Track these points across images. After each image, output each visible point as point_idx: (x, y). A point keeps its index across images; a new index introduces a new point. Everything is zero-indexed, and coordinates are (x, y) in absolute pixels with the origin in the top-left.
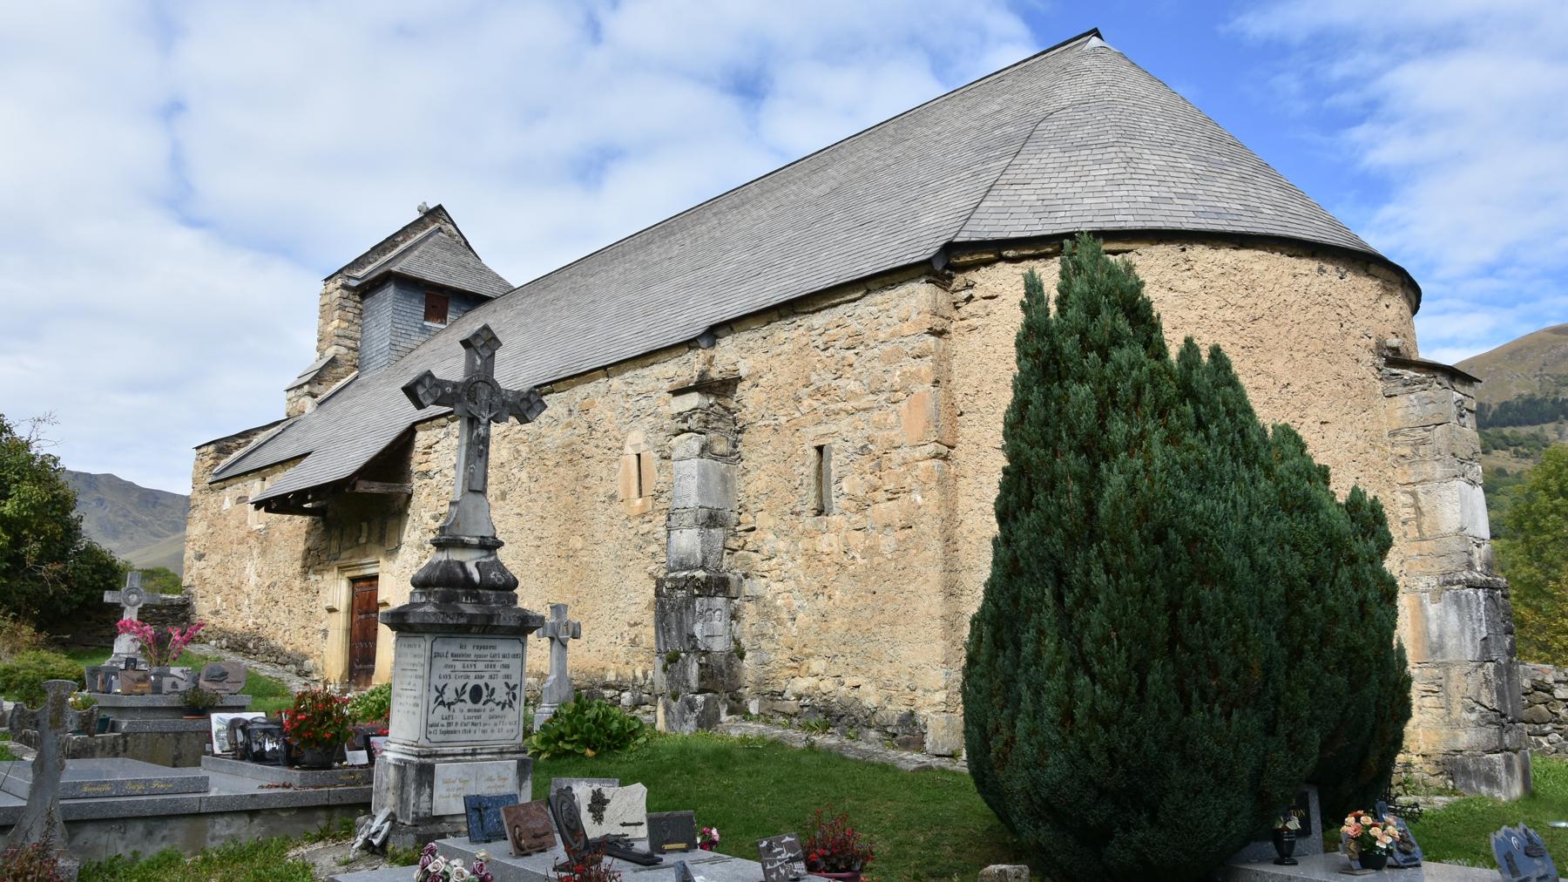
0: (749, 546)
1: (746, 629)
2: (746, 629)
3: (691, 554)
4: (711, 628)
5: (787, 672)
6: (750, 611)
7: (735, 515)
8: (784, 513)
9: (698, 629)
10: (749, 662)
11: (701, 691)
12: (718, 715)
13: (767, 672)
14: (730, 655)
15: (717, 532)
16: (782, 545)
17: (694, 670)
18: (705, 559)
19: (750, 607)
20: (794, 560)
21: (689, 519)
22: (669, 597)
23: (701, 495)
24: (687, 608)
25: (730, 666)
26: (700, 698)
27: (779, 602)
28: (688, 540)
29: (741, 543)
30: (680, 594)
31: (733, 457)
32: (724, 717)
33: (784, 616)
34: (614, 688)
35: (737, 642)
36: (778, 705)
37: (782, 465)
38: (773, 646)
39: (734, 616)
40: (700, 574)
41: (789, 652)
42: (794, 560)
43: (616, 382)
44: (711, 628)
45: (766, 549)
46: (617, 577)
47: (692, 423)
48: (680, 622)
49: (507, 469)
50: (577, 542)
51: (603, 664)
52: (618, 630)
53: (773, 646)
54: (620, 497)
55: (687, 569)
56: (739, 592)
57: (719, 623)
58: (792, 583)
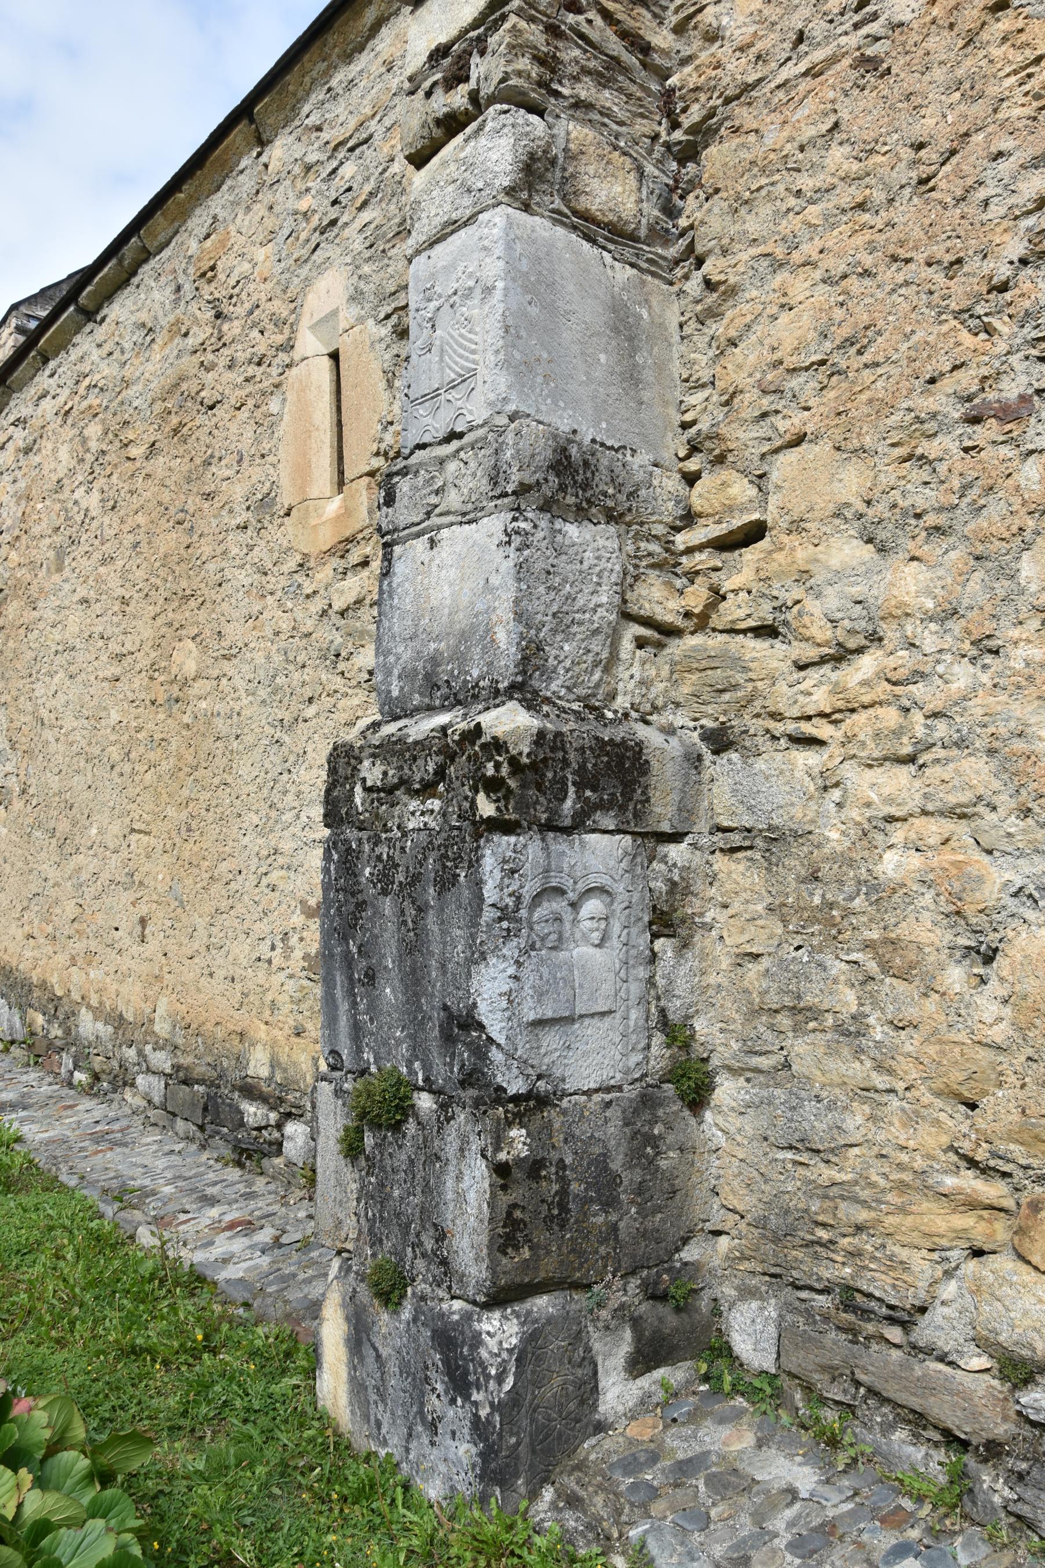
0: (733, 610)
1: (716, 983)
2: (716, 983)
3: (476, 633)
4: (562, 984)
5: (944, 1222)
6: (735, 897)
7: (673, 483)
8: (926, 425)
9: (490, 989)
10: (730, 1121)
11: (500, 1297)
12: (589, 1390)
13: (826, 1191)
14: (647, 1101)
15: (592, 542)
16: (910, 583)
17: (468, 1192)
18: (532, 655)
19: (737, 874)
20: (987, 648)
21: (465, 478)
22: (375, 827)
23: (521, 369)
24: (446, 882)
25: (644, 1145)
26: (499, 1332)
27: (893, 864)
28: (463, 576)
29: (696, 597)
30: (419, 815)
31: (657, 244)
32: (617, 1392)
33: (924, 929)
34: (262, 1098)
35: (675, 1032)
36: (883, 1362)
37: (908, 213)
38: (859, 1070)
39: (666, 921)
40: (509, 721)
41: (955, 1121)
42: (987, 648)
43: (281, 151)
44: (562, 984)
45: (818, 619)
46: (275, 758)
47: (486, 71)
48: (413, 946)
49: (66, 494)
50: (187, 659)
51: (241, 1020)
52: (276, 923)
53: (859, 1070)
54: (285, 499)
55: (455, 701)
56: (687, 810)
57: (595, 955)
58: (976, 772)
